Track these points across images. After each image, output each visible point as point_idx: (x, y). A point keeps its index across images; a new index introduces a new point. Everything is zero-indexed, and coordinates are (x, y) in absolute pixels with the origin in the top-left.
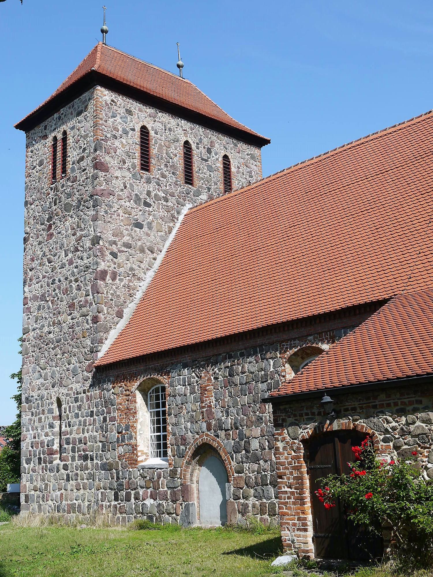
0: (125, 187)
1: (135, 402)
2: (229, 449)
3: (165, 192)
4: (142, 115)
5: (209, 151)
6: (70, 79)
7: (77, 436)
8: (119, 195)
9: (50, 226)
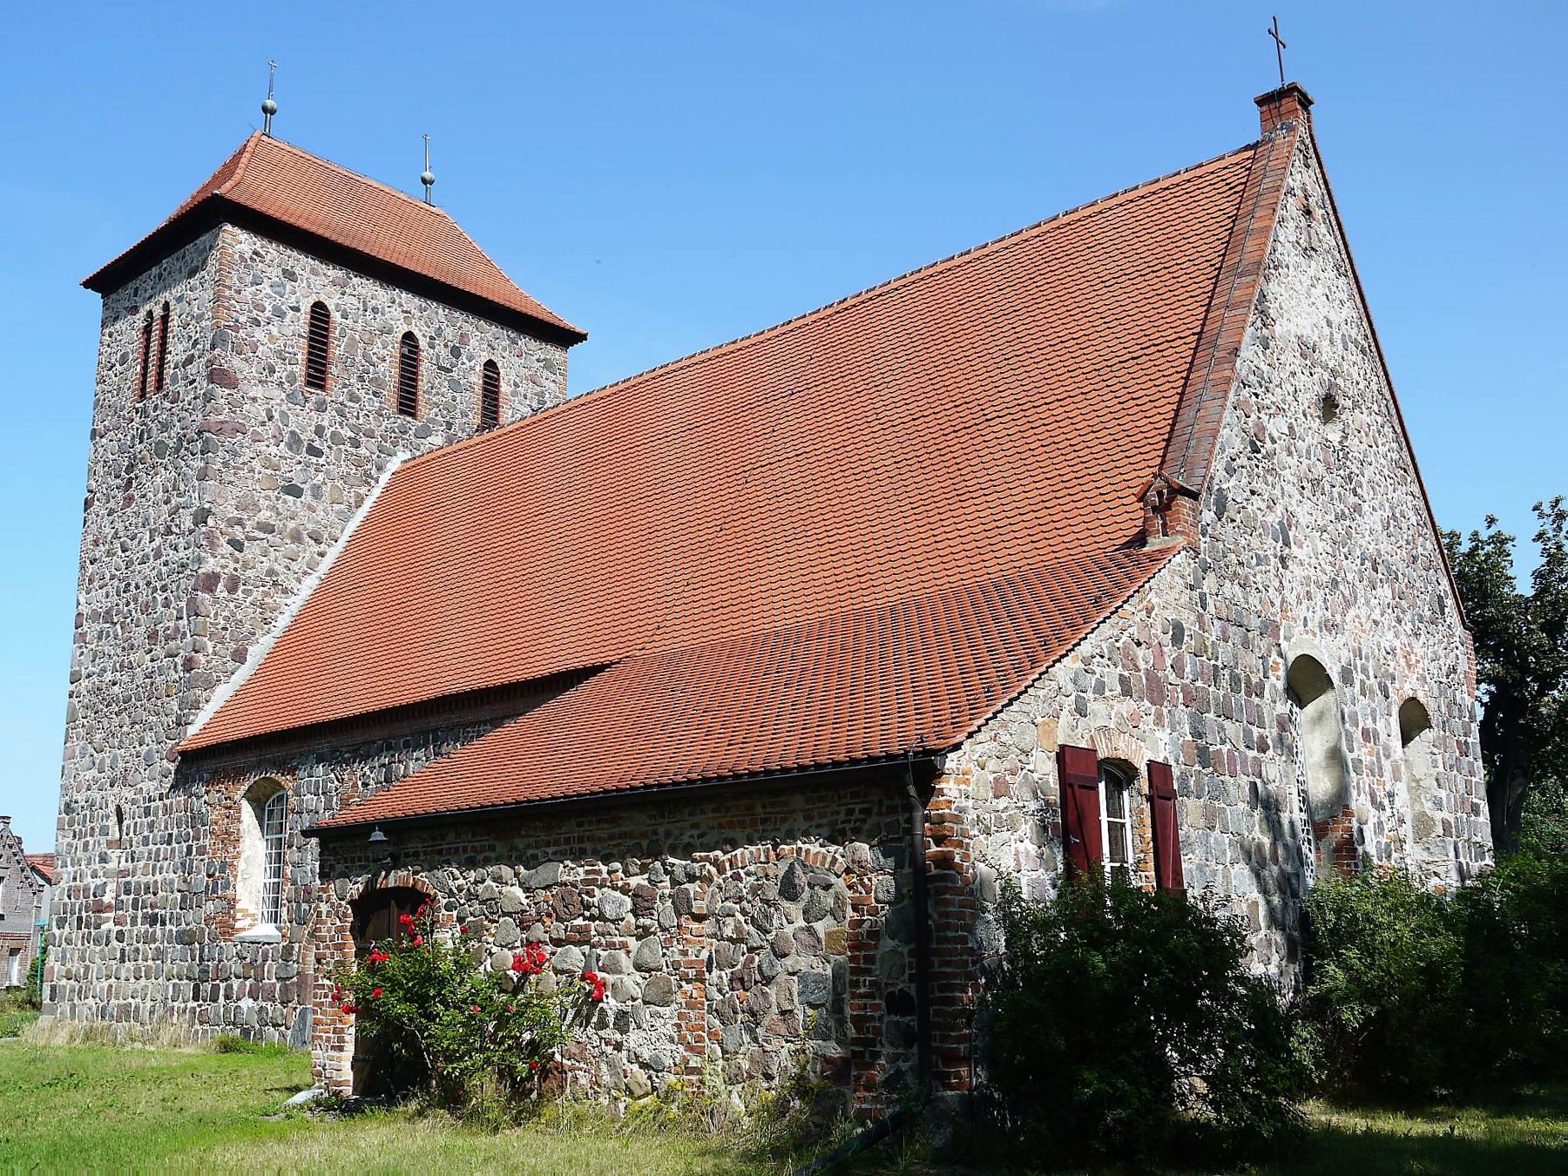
0: (271, 418)
1: (239, 821)
3: (355, 428)
4: (318, 281)
5: (456, 352)
6: (193, 198)
7: (144, 880)
9: (130, 481)
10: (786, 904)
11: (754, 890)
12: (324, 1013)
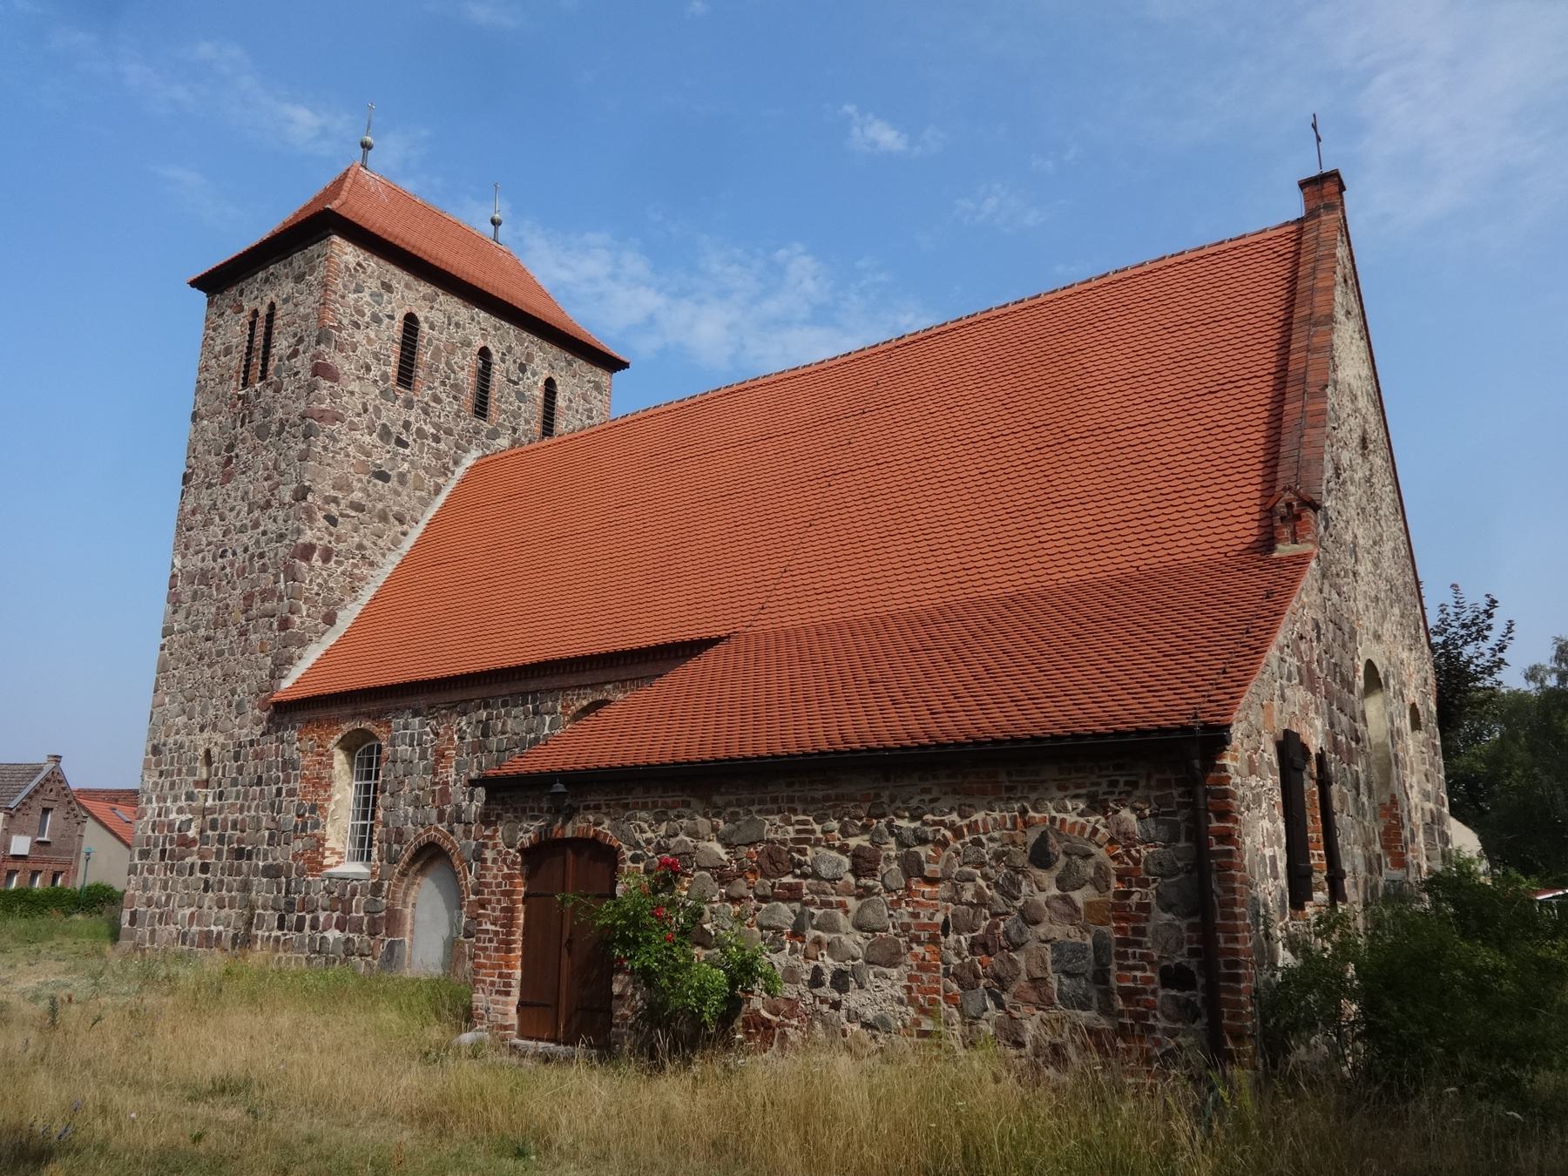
0: (366, 411)
2: (467, 854)
3: (437, 426)
4: (410, 295)
5: (523, 368)
6: (296, 216)
8: (351, 422)
9: (229, 460)
10: (1038, 872)
11: (998, 856)
12: (488, 957)
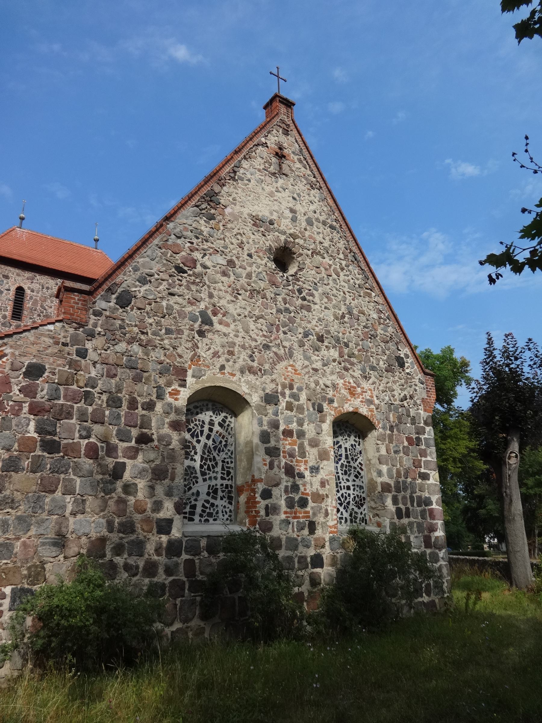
4: (20, 278)
